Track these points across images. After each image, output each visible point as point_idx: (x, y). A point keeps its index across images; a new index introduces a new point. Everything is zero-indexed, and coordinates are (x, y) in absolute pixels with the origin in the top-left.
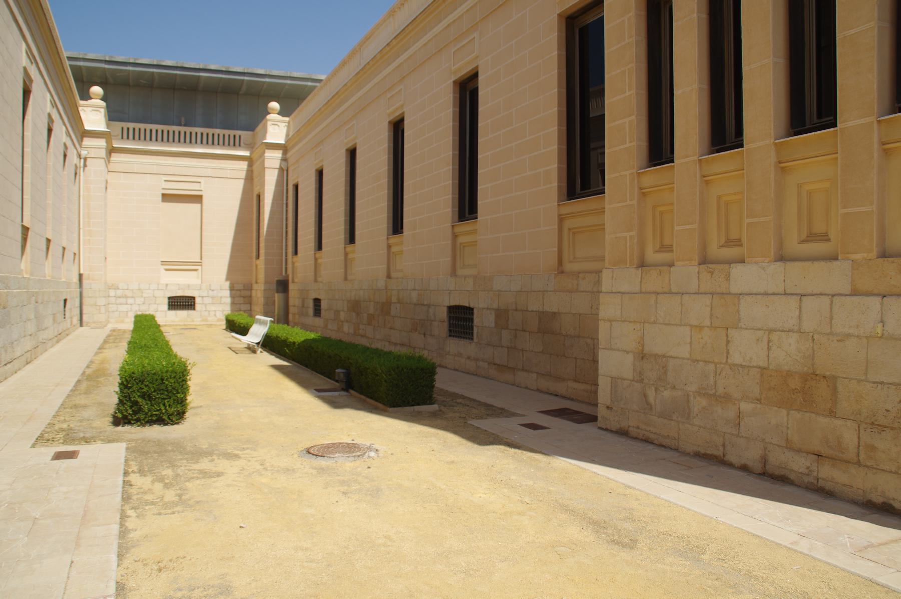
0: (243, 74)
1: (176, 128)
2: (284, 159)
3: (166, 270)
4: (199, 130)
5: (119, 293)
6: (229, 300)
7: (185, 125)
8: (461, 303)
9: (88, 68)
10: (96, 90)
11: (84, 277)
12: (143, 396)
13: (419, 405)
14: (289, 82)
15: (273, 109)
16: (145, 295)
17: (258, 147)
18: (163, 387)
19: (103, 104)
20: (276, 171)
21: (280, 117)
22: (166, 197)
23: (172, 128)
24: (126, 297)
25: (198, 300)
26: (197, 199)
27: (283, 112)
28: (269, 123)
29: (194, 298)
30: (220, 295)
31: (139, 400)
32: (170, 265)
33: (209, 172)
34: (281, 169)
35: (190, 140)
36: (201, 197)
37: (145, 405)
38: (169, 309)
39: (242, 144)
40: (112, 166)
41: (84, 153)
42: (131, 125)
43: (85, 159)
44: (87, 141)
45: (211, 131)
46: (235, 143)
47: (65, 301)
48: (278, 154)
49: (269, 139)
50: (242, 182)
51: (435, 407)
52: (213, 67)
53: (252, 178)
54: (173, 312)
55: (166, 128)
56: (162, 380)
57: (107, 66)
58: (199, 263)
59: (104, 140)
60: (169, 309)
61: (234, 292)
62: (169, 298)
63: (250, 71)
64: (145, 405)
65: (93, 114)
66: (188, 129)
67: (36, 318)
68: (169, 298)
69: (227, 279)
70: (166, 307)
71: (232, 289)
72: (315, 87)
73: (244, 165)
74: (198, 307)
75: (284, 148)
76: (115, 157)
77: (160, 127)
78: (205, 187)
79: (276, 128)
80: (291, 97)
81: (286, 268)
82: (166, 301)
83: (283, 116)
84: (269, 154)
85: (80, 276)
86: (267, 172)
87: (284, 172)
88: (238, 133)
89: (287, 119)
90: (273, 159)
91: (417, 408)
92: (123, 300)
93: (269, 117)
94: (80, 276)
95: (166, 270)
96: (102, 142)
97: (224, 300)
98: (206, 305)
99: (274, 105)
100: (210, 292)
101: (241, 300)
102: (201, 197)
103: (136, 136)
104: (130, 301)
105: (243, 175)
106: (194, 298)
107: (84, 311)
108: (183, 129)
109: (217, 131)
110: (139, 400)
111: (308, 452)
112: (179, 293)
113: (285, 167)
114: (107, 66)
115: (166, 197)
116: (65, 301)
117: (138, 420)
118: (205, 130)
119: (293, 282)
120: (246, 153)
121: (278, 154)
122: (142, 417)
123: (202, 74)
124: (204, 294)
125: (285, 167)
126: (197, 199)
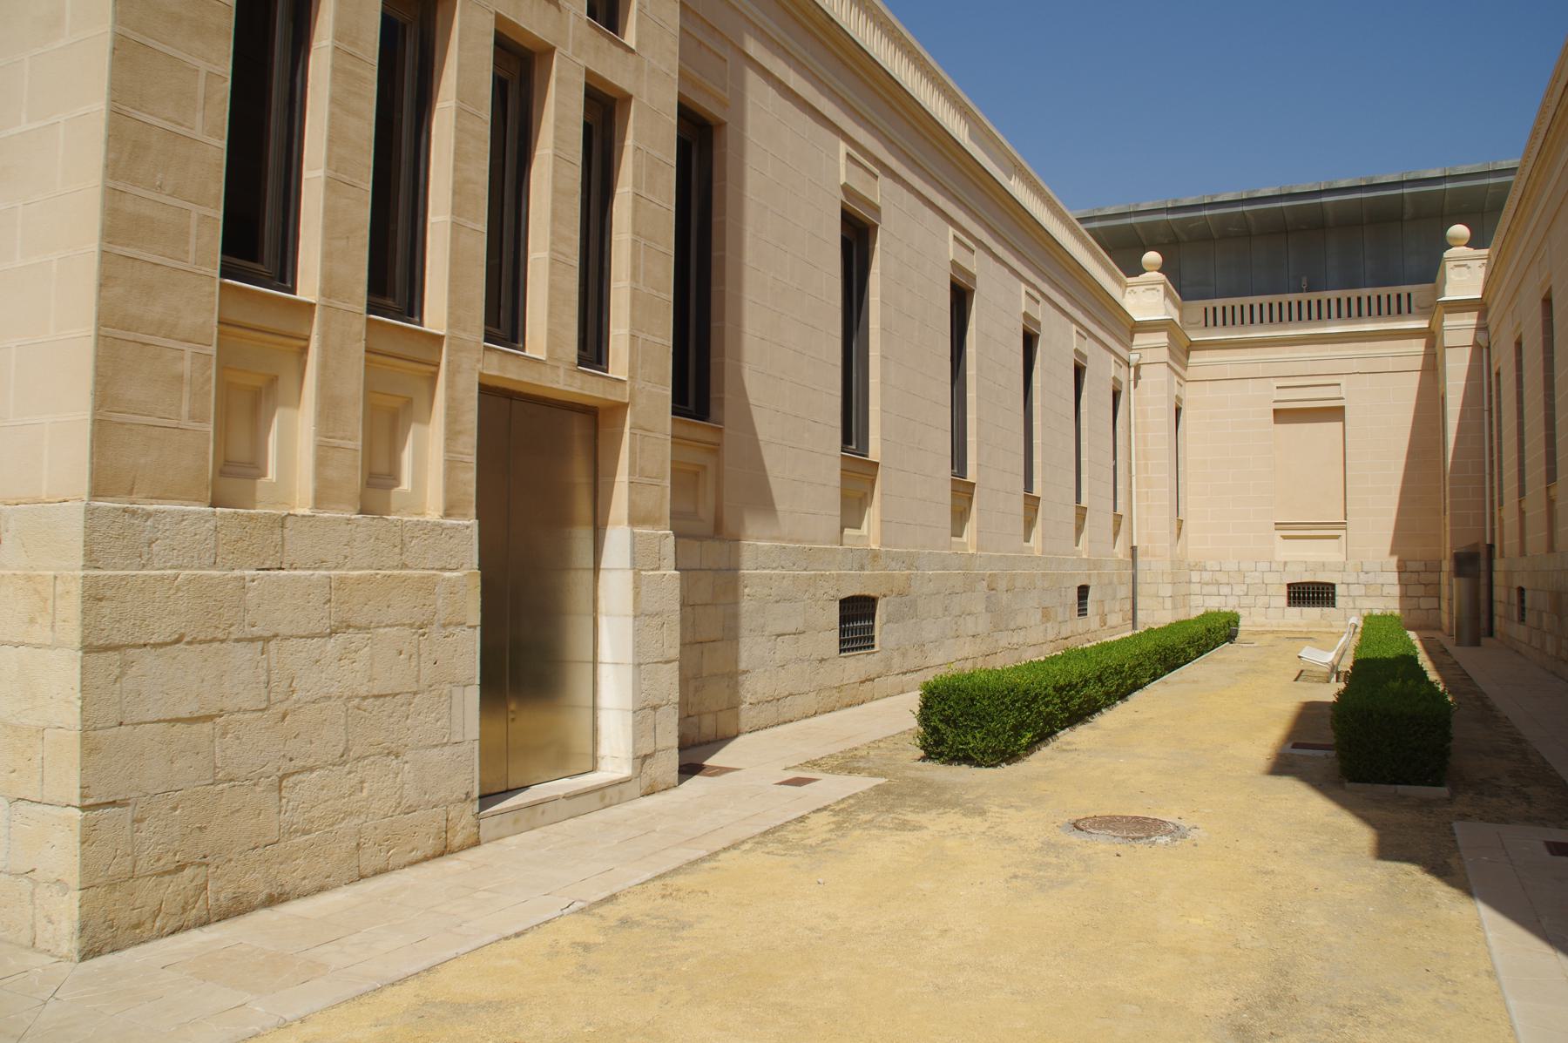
0: (1400, 184)
1: (1294, 297)
2: (1482, 328)
3: (1285, 537)
4: (1333, 295)
5: (1207, 576)
6: (1396, 590)
7: (1308, 290)
8: (857, 593)
9: (1143, 224)
10: (1152, 257)
11: (1139, 551)
12: (947, 720)
13: (1408, 783)
14: (1492, 181)
15: (1456, 239)
16: (1248, 580)
17: (1438, 309)
18: (972, 711)
19: (1162, 277)
20: (1468, 351)
21: (1471, 251)
22: (1281, 416)
23: (1285, 298)
24: (1218, 584)
25: (1339, 590)
26: (1335, 413)
27: (1474, 243)
28: (1449, 265)
29: (1333, 585)
30: (1380, 580)
31: (942, 726)
32: (1290, 530)
33: (1355, 366)
34: (1476, 346)
35: (1320, 313)
36: (1343, 408)
37: (949, 734)
38: (1289, 604)
39: (1413, 309)
40: (1190, 373)
41: (1134, 358)
42: (1219, 303)
43: (1137, 367)
44: (1140, 340)
45: (1353, 294)
46: (1401, 308)
47: (1083, 591)
48: (1470, 319)
49: (1450, 294)
50: (1416, 377)
51: (1443, 791)
52: (1343, 184)
53: (1432, 368)
54: (1296, 610)
55: (1275, 299)
56: (972, 700)
57: (1170, 217)
58: (1342, 525)
59: (1165, 334)
60: (1289, 604)
61: (1405, 576)
62: (1289, 585)
63: (1411, 177)
64: (949, 734)
65: (1147, 297)
66: (1314, 297)
67: (987, 610)
68: (1289, 585)
69: (1392, 553)
70: (1284, 600)
71: (1402, 569)
72: (1510, 183)
73: (1418, 346)
74: (1339, 601)
75: (1480, 306)
76: (1196, 357)
77: (1265, 299)
78: (1348, 393)
79: (1464, 273)
80: (1481, 209)
81: (1492, 530)
82: (1285, 591)
83: (1476, 248)
84: (1450, 321)
85: (1134, 549)
86: (1450, 355)
87: (1481, 350)
88: (1404, 290)
89: (1485, 252)
90: (1460, 331)
91: (1401, 788)
92: (1213, 589)
93: (1446, 255)
94: (1134, 549)
95: (1285, 537)
96: (1162, 338)
97: (1386, 590)
98: (1354, 597)
99: (1459, 230)
100: (1362, 575)
101: (1421, 590)
102: (1343, 408)
103: (1227, 319)
104: (1225, 590)
105: (1418, 363)
106: (1333, 585)
107: (1139, 606)
108: (1304, 297)
109: (1365, 292)
110: (942, 726)
111: (1076, 826)
112: (1307, 578)
113: (1483, 343)
114: (1170, 217)
115: (1281, 416)
116: (1083, 591)
117: (941, 755)
118: (1343, 294)
119: (1502, 556)
120: (1424, 324)
121: (1470, 319)
122: (946, 751)
123: (1324, 199)
124: (1352, 579)
125: (1483, 343)
126: (1335, 413)
